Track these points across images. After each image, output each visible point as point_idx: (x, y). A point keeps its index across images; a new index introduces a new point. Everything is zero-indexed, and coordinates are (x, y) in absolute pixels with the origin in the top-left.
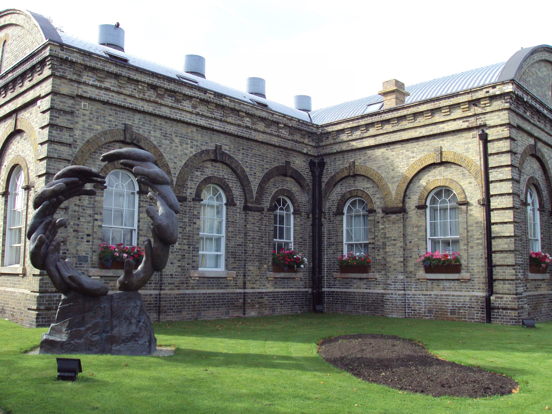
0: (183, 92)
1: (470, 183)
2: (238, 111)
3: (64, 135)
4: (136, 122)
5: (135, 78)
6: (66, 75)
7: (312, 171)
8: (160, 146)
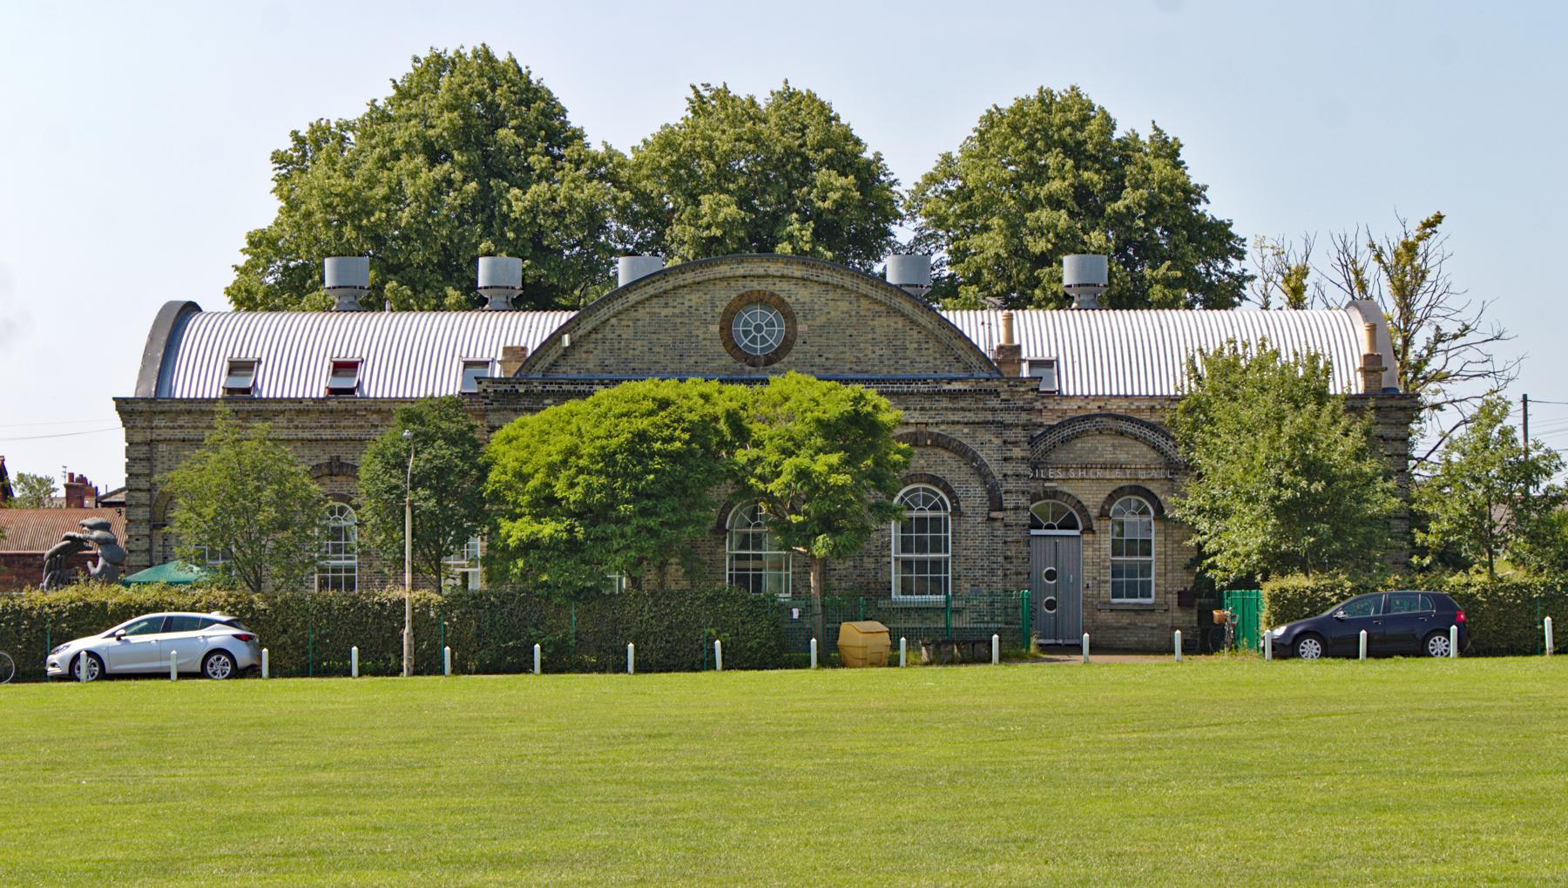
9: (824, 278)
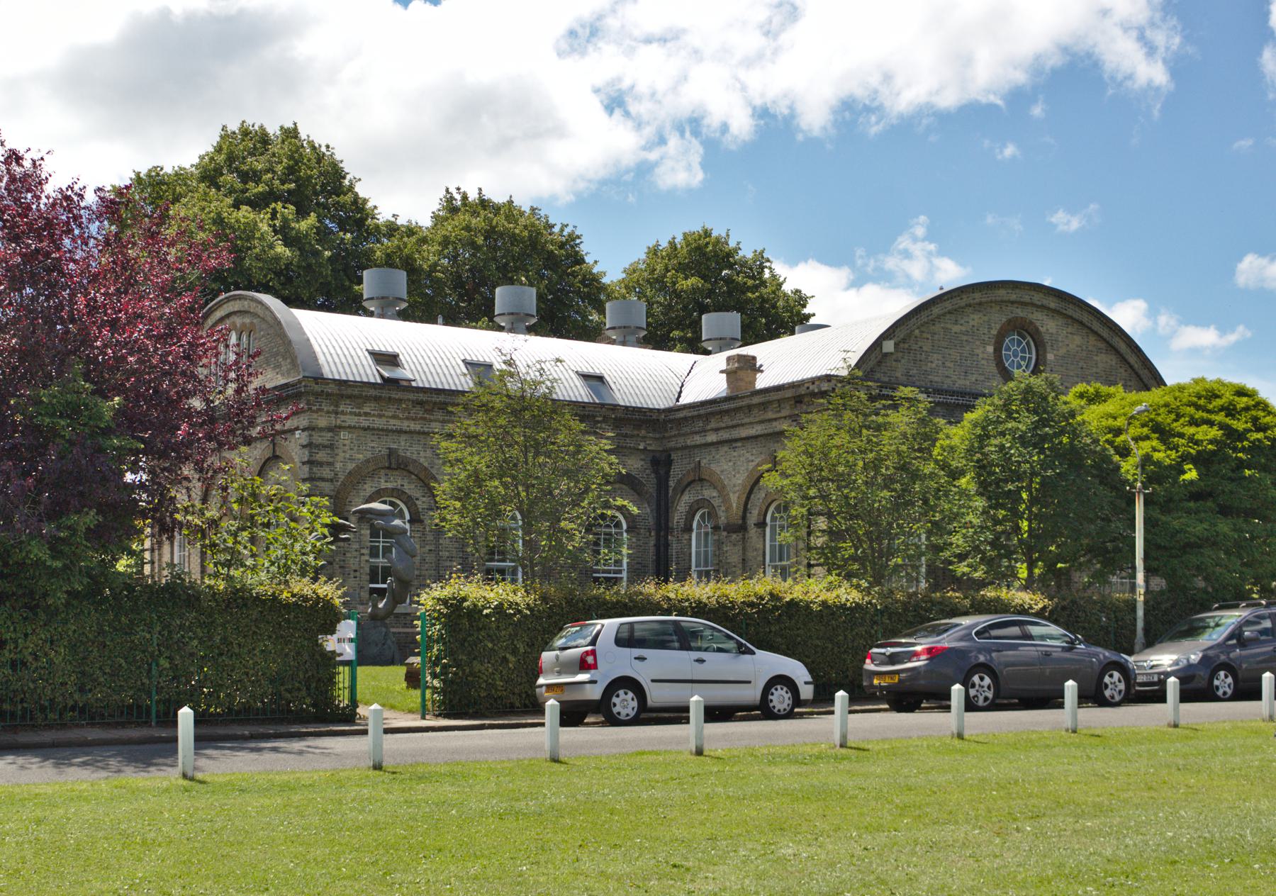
7: (656, 472)
9: (1070, 312)
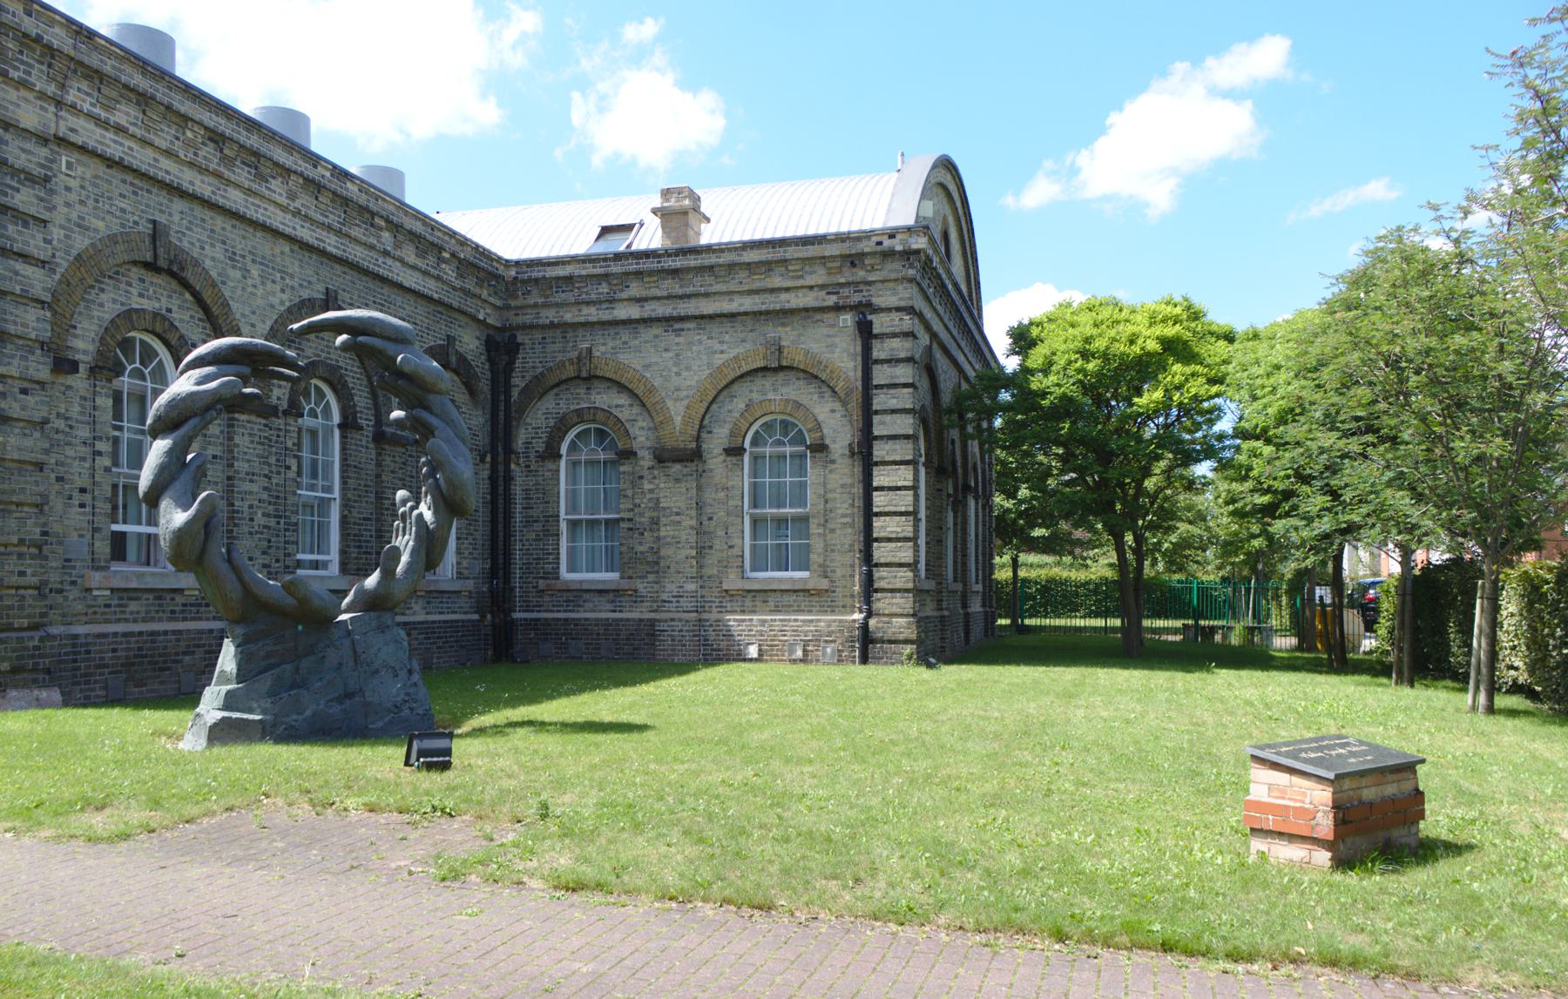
0: (275, 157)
1: (833, 411)
2: (373, 214)
3: (33, 237)
4: (176, 218)
5: (183, 110)
6: (33, 80)
7: (490, 360)
8: (224, 283)
